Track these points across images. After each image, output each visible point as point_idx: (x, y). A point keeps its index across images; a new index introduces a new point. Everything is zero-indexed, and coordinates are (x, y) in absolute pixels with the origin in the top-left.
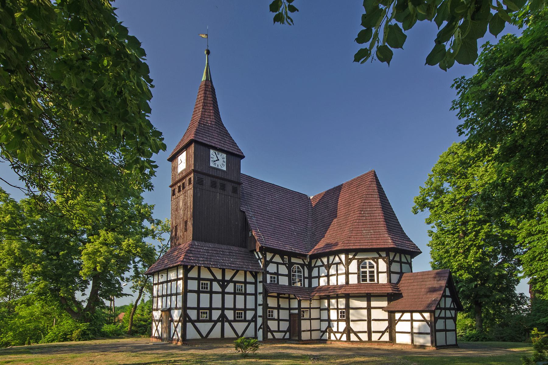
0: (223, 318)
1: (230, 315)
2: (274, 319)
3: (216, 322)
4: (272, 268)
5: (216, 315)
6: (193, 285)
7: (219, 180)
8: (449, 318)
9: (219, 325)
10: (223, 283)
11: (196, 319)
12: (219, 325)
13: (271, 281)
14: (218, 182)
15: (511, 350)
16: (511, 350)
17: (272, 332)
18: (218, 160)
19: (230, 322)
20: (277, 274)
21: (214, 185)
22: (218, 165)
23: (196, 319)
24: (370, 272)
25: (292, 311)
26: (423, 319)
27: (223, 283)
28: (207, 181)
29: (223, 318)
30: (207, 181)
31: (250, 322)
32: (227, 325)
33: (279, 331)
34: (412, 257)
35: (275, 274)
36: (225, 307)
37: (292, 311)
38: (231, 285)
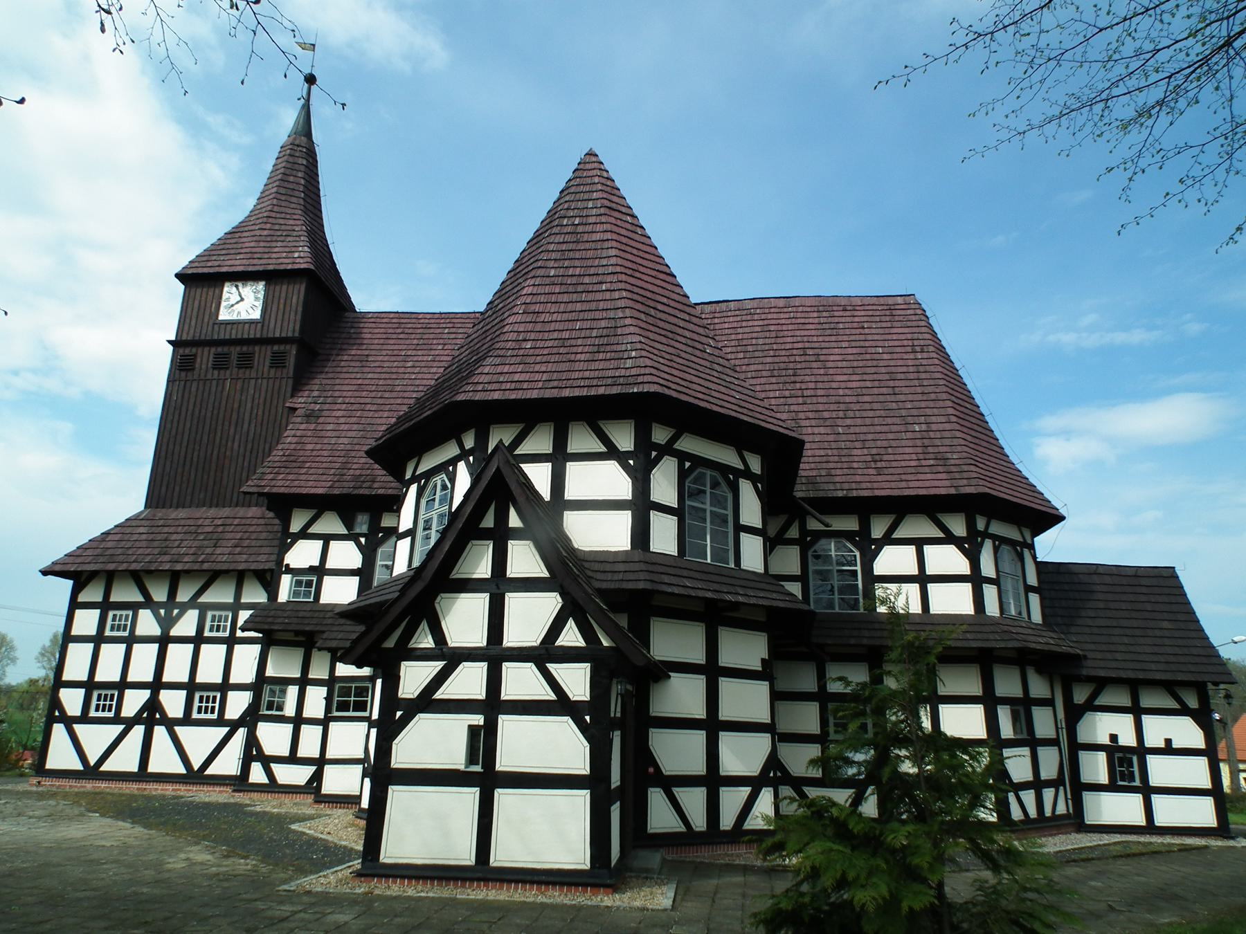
0: (152, 715)
1: (173, 703)
2: (282, 719)
3: (130, 724)
4: (303, 554)
5: (134, 702)
6: (86, 621)
7: (232, 349)
8: (1025, 786)
9: (139, 730)
10: (169, 613)
11: (180, 715)
12: (139, 730)
13: (296, 594)
14: (235, 351)
15: (730, 614)
16: (730, 614)
17: (267, 761)
18: (242, 300)
19: (170, 724)
20: (320, 571)
21: (221, 363)
22: (239, 313)
23: (180, 715)
24: (840, 593)
25: (293, 691)
26: (552, 696)
27: (169, 613)
28: (205, 358)
29: (152, 715)
30: (205, 358)
31: (234, 726)
32: (160, 732)
33: (293, 758)
34: (1038, 531)
35: (312, 570)
36: (930, 586)
37: (293, 691)
38: (192, 616)
